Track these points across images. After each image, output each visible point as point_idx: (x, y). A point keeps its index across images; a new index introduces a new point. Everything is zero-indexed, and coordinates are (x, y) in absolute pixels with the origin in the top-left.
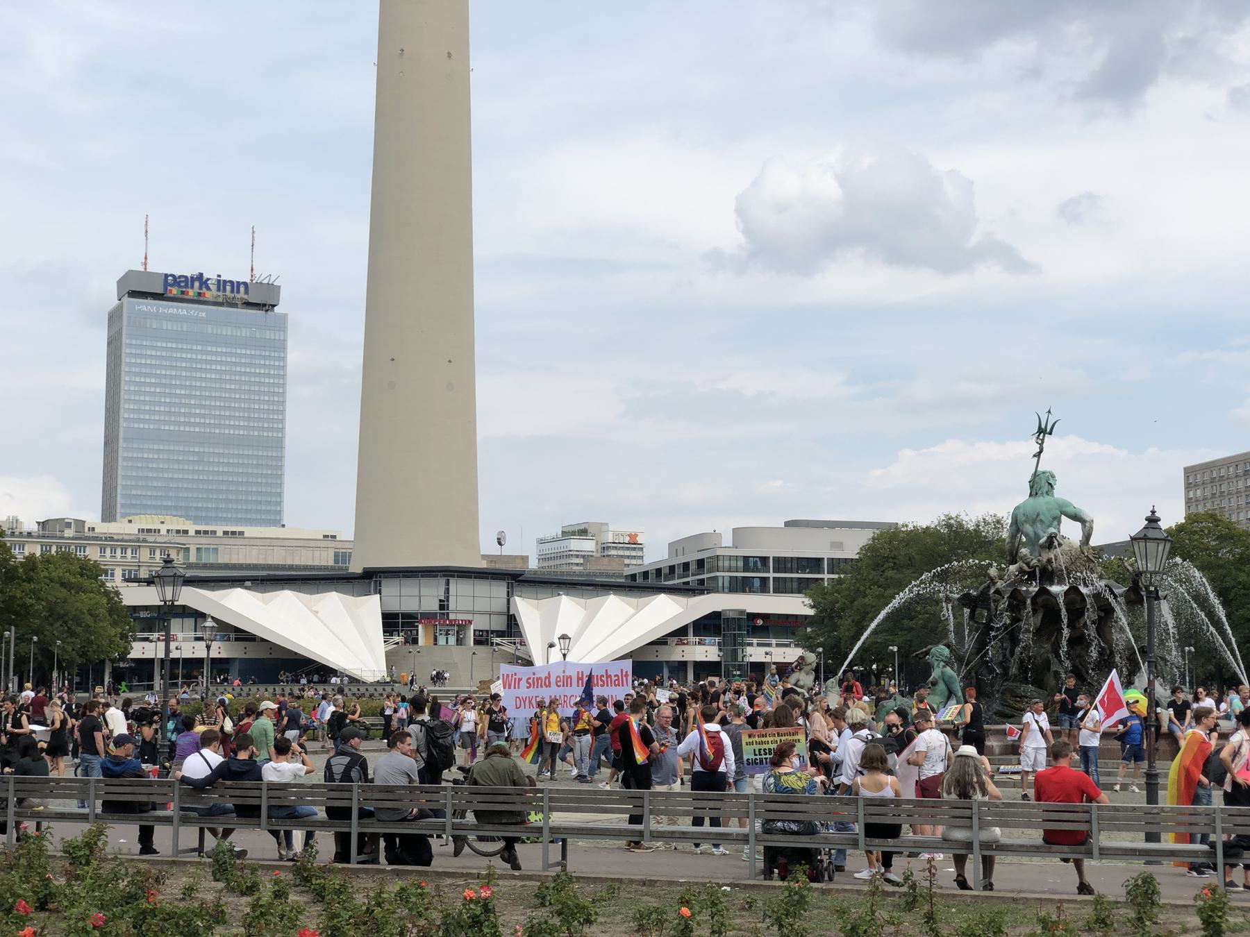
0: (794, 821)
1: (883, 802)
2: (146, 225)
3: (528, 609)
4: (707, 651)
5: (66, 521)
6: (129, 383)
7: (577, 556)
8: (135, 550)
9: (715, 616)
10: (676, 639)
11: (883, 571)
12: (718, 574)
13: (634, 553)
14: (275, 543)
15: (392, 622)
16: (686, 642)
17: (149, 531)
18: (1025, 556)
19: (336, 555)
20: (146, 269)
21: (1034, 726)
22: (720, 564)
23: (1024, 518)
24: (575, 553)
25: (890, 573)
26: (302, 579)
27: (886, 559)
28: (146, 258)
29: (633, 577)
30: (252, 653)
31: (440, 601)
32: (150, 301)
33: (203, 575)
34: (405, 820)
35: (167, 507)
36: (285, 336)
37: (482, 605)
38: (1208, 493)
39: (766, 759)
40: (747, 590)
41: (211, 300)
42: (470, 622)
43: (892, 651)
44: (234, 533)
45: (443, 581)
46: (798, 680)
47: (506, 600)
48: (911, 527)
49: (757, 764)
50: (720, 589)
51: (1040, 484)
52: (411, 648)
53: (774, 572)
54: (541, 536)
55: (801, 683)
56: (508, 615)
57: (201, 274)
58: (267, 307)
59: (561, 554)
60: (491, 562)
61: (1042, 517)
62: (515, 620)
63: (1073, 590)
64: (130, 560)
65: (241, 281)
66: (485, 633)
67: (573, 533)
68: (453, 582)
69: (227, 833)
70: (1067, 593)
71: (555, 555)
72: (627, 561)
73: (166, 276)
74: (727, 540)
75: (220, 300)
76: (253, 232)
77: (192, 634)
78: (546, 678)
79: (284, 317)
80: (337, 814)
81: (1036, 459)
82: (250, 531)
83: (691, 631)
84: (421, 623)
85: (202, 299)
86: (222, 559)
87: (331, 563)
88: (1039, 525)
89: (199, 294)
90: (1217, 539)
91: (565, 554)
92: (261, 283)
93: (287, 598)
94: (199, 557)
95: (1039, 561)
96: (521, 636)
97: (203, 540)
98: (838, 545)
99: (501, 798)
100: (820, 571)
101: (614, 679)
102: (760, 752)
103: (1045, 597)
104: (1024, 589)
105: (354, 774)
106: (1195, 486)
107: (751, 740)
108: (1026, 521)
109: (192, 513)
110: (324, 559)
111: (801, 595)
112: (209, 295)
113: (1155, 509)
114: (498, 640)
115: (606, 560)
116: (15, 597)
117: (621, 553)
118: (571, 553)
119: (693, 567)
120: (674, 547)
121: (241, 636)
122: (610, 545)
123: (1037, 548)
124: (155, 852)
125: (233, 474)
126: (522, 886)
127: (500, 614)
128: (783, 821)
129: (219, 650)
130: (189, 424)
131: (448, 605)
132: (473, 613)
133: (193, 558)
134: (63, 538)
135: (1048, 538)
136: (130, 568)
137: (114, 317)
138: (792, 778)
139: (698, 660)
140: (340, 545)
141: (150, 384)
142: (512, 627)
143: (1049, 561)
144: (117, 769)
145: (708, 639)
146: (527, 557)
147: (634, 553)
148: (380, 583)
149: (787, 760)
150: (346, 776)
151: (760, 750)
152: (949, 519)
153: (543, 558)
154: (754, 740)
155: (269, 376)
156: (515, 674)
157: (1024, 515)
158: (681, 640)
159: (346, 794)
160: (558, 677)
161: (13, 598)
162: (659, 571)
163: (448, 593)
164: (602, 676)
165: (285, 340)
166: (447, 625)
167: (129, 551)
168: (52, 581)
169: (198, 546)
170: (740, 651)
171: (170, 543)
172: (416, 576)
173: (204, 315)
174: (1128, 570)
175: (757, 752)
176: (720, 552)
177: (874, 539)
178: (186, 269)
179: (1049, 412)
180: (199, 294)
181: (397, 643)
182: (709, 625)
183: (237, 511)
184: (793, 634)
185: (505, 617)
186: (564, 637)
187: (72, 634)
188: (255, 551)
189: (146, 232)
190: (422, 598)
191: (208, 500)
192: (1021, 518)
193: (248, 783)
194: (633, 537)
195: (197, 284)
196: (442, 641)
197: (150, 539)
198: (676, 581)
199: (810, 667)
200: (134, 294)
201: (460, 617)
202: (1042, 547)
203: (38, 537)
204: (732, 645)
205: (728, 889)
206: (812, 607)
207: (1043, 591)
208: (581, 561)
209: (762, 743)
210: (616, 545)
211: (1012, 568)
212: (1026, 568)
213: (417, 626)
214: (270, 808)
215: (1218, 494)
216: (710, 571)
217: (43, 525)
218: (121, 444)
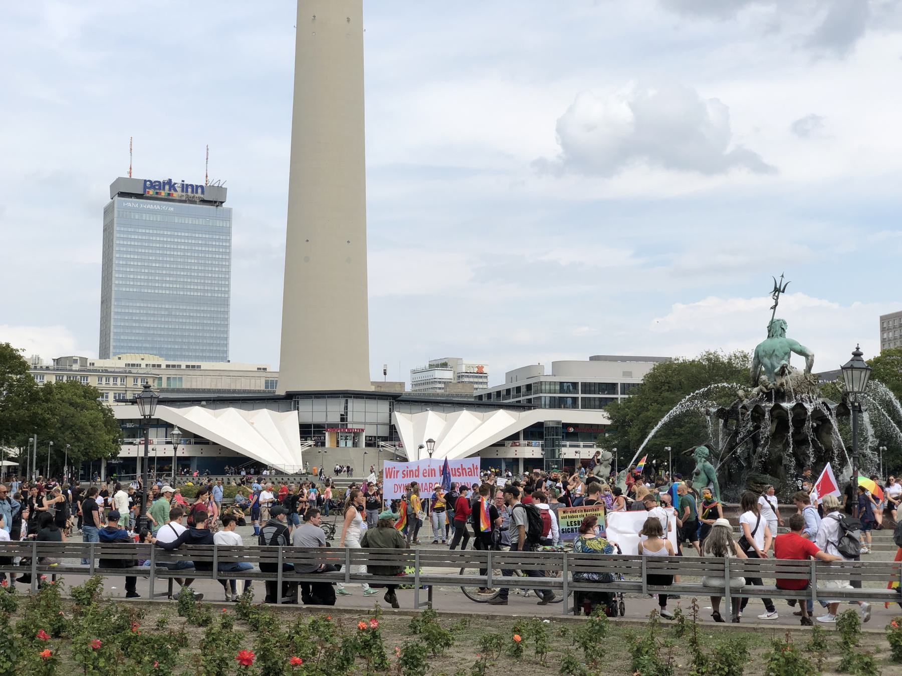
0: (596, 573)
1: (660, 560)
3: (404, 421)
4: (533, 451)
6: (119, 258)
7: (440, 382)
8: (123, 379)
9: (540, 425)
10: (511, 442)
13: (480, 380)
14: (222, 373)
15: (306, 431)
16: (518, 444)
17: (133, 365)
19: (267, 382)
20: (130, 176)
22: (543, 387)
23: (763, 354)
24: (226, 373)
25: (666, 394)
26: (243, 400)
27: (663, 384)
28: (131, 169)
29: (480, 397)
30: (206, 452)
31: (341, 415)
32: (134, 200)
33: (172, 397)
34: (316, 572)
35: (146, 348)
36: (230, 224)
37: (371, 418)
39: (576, 528)
40: (563, 406)
41: (177, 198)
42: (363, 430)
43: (667, 450)
44: (193, 367)
45: (343, 401)
46: (599, 472)
47: (388, 415)
48: (681, 361)
50: (543, 406)
51: (776, 329)
52: (320, 449)
53: (582, 393)
54: (414, 368)
55: (601, 474)
57: (170, 180)
58: (217, 203)
59: (428, 381)
60: (378, 386)
61: (776, 352)
62: (395, 429)
63: (800, 406)
65: (199, 184)
66: (373, 439)
67: (437, 366)
68: (350, 401)
69: (189, 582)
70: (793, 409)
71: (424, 382)
72: (476, 386)
73: (145, 181)
74: (548, 370)
75: (184, 198)
77: (164, 439)
78: (416, 470)
79: (229, 211)
80: (268, 568)
81: (773, 310)
82: (205, 365)
83: (522, 436)
84: (327, 431)
85: (170, 197)
86: (185, 385)
87: (263, 388)
88: (774, 359)
89: (169, 194)
91: (432, 380)
93: (231, 413)
94: (169, 384)
95: (774, 384)
96: (399, 440)
97: (172, 372)
98: (628, 374)
99: (385, 557)
100: (615, 392)
101: (467, 471)
102: (571, 523)
103: (778, 411)
105: (280, 539)
107: (565, 515)
108: (765, 356)
110: (258, 385)
111: (601, 410)
112: (176, 195)
114: (382, 443)
115: (460, 385)
116: (37, 413)
117: (472, 380)
118: (436, 380)
119: (523, 390)
120: (510, 375)
121: (199, 440)
122: (463, 374)
123: (773, 375)
126: (400, 620)
127: (384, 424)
128: (588, 573)
130: (162, 288)
131: (347, 418)
132: (365, 423)
134: (71, 370)
135: (781, 368)
137: (108, 211)
138: (594, 542)
141: (134, 260)
142: (393, 434)
143: (782, 385)
144: (111, 536)
145: (534, 442)
146: (404, 383)
147: (480, 380)
148: (298, 403)
149: (591, 529)
150: (274, 541)
151: (571, 522)
152: (709, 354)
153: (415, 384)
154: (567, 515)
156: (394, 468)
157: (763, 351)
158: (515, 443)
159: (274, 554)
160: (426, 470)
161: (35, 414)
163: (347, 409)
164: (459, 469)
165: (230, 227)
166: (346, 433)
167: (119, 380)
169: (168, 376)
170: (557, 451)
171: (148, 374)
172: (324, 397)
174: (839, 391)
176: (542, 379)
177: (654, 369)
179: (782, 276)
181: (310, 446)
182: (535, 432)
183: (195, 350)
184: (596, 438)
185: (388, 427)
186: (430, 441)
187: (78, 440)
188: (208, 379)
189: (131, 149)
190: (318, 413)
191: (175, 343)
192: (761, 353)
193: (204, 546)
194: (480, 368)
195: (167, 187)
196: (342, 443)
197: (134, 370)
198: (511, 400)
199: (607, 462)
200: (122, 194)
201: (356, 427)
202: (777, 374)
203: (54, 370)
204: (551, 446)
205: (548, 621)
206: (609, 419)
207: (777, 407)
208: (443, 386)
209: (573, 517)
210: (468, 374)
211: (755, 390)
213: (325, 434)
214: (219, 563)
216: (536, 393)
217: (57, 361)
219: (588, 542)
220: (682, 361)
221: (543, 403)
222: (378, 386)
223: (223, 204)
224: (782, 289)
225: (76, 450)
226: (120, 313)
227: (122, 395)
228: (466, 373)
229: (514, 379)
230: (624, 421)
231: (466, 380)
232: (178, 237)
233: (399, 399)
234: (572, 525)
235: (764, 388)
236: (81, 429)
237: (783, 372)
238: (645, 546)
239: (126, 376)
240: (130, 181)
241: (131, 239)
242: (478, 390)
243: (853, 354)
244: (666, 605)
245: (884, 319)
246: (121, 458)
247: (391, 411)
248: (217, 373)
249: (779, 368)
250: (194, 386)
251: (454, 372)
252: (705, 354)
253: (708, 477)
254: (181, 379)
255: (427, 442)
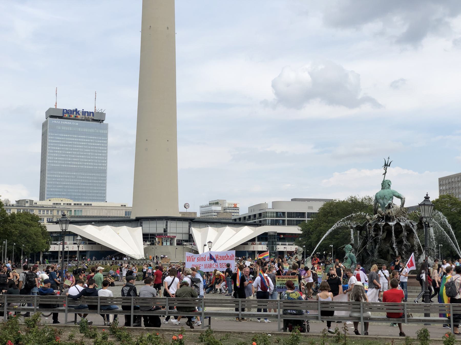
0: (294, 310)
1: (327, 303)
2: (56, 91)
3: (196, 232)
4: (262, 247)
5: (26, 200)
7: (215, 212)
9: (266, 234)
10: (251, 243)
11: (328, 217)
12: (267, 218)
13: (235, 211)
15: (146, 237)
16: (255, 244)
17: (57, 204)
18: (380, 211)
19: (126, 212)
20: (56, 107)
21: (382, 275)
22: (267, 215)
23: (380, 197)
25: (330, 218)
26: (113, 221)
27: (329, 213)
28: (56, 103)
29: (235, 220)
30: (95, 249)
31: (164, 229)
32: (58, 119)
34: (151, 310)
36: (107, 131)
37: (179, 230)
38: (447, 187)
39: (284, 287)
40: (277, 224)
41: (80, 118)
43: (331, 246)
44: (88, 204)
45: (165, 222)
48: (337, 201)
49: (281, 288)
50: (267, 224)
51: (385, 185)
52: (153, 246)
53: (307, 218)
54: (202, 205)
56: (189, 234)
57: (76, 109)
58: (100, 121)
59: (209, 212)
60: (183, 214)
61: (386, 197)
62: (192, 236)
63: (398, 224)
64: (49, 215)
66: (180, 241)
67: (213, 204)
69: (85, 315)
70: (395, 225)
71: (207, 212)
72: (233, 214)
73: (64, 110)
74: (270, 206)
75: (83, 119)
76: (96, 94)
77: (72, 242)
78: (204, 257)
79: (107, 125)
80: (126, 308)
81: (384, 175)
82: (94, 204)
83: (257, 240)
84: (157, 237)
86: (84, 214)
87: (124, 215)
88: (385, 200)
89: (76, 117)
90: (451, 204)
92: (98, 112)
93: (108, 228)
95: (385, 213)
97: (77, 207)
98: (311, 208)
99: (186, 302)
100: (304, 217)
101: (230, 257)
102: (282, 284)
103: (387, 226)
104: (380, 223)
106: (443, 185)
107: (279, 279)
108: (380, 199)
109: (73, 197)
110: (122, 214)
112: (79, 117)
113: (428, 194)
114: (185, 243)
115: (225, 214)
117: (231, 211)
118: (212, 211)
119: (257, 216)
120: (251, 209)
121: (91, 242)
124: (59, 323)
125: (88, 183)
126: (194, 334)
128: (290, 310)
129: (82, 248)
131: (167, 231)
132: (176, 233)
133: (73, 214)
134: (25, 207)
135: (388, 205)
136: (50, 218)
137: (45, 125)
139: (259, 250)
140: (127, 209)
141: (57, 150)
142: (190, 239)
143: (389, 213)
144: (45, 292)
145: (263, 243)
147: (235, 211)
148: (142, 223)
151: (282, 283)
152: (352, 198)
153: (202, 213)
154: (280, 279)
155: (101, 146)
158: (253, 243)
161: (6, 229)
162: (245, 218)
164: (225, 256)
165: (107, 133)
166: (167, 238)
167: (49, 211)
168: (21, 222)
169: (75, 209)
170: (275, 247)
173: (77, 124)
175: (281, 284)
176: (267, 211)
177: (324, 205)
178: (71, 107)
179: (389, 158)
180: (76, 117)
181: (148, 245)
182: (263, 238)
183: (89, 196)
185: (188, 235)
186: (210, 242)
187: (28, 242)
188: (96, 211)
189: (56, 94)
190: (152, 228)
191: (79, 192)
192: (378, 197)
193: (93, 297)
194: (235, 205)
195: (75, 113)
196: (165, 244)
197: (57, 207)
198: (251, 221)
200: (52, 117)
201: (171, 235)
202: (386, 208)
203: (16, 206)
205: (270, 335)
206: (301, 231)
207: (387, 224)
208: (216, 214)
209: (283, 281)
210: (229, 208)
212: (380, 216)
213: (156, 238)
214: (101, 306)
215: (451, 188)
216: (264, 217)
217: (18, 202)
218: (47, 172)
219: (291, 294)
220: (338, 201)
221: (267, 222)
222: (183, 214)
223: (104, 121)
224: (388, 165)
225: (27, 247)
226: (50, 177)
227: (51, 219)
228: (228, 207)
229: (253, 211)
230: (309, 231)
231: (228, 211)
232: (80, 138)
233: (193, 221)
234: (282, 285)
235: (380, 215)
236: (30, 237)
237: (389, 207)
238: (320, 296)
239: (53, 210)
240: (56, 109)
241: (56, 140)
242: (234, 216)
243: (425, 198)
244: (330, 326)
245: (440, 180)
246: (51, 252)
247: (189, 227)
248: (100, 208)
249: (387, 205)
250: (88, 214)
251: (222, 207)
252: (349, 197)
253: (352, 260)
254: (81, 211)
255: (208, 243)
